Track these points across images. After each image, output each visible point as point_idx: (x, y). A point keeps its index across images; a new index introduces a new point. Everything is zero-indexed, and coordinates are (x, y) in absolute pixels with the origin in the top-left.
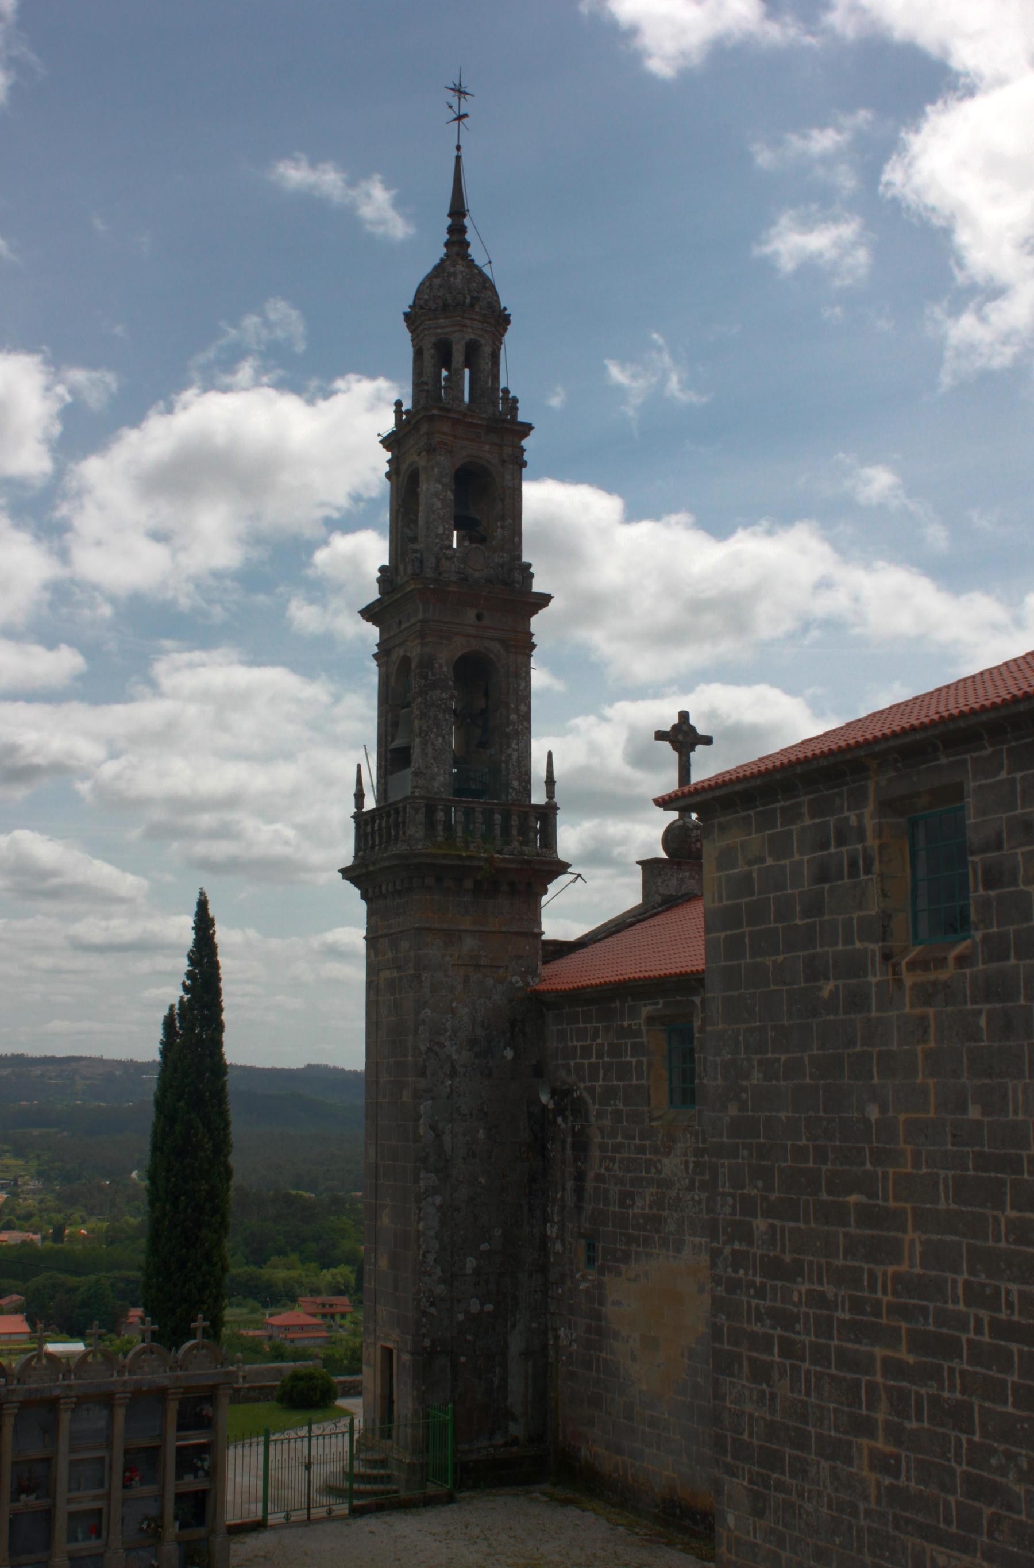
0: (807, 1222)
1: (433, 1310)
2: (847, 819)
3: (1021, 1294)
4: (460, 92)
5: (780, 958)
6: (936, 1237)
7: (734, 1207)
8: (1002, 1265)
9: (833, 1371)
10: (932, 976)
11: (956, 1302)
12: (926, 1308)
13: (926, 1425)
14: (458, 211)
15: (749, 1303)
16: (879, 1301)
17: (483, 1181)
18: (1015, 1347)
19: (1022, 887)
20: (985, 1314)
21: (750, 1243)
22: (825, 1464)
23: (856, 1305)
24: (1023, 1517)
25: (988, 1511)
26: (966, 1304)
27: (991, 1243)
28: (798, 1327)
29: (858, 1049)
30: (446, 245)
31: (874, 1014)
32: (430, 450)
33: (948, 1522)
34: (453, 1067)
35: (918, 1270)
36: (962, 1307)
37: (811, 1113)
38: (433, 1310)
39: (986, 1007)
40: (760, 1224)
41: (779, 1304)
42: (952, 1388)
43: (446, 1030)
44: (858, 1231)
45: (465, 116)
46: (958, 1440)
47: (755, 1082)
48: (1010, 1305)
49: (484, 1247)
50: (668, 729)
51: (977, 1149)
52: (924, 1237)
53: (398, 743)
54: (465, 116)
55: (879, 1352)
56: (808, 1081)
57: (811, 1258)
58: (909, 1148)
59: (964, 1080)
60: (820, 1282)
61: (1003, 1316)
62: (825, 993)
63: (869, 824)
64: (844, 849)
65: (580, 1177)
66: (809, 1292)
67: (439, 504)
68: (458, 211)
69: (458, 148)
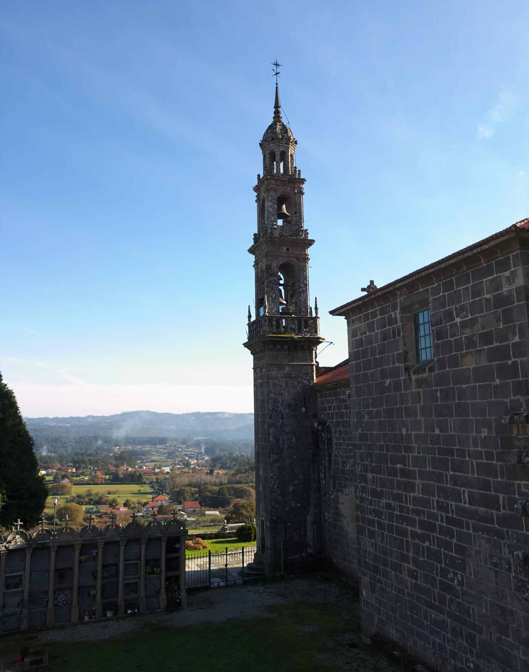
0: (384, 475)
1: (277, 506)
2: (391, 315)
3: (456, 506)
4: (277, 65)
5: (372, 371)
6: (426, 482)
7: (361, 469)
8: (449, 494)
9: (395, 536)
10: (421, 376)
11: (465, 503)
12: (424, 511)
13: (426, 559)
15: (367, 507)
16: (408, 507)
17: (295, 457)
19: (449, 339)
20: (443, 514)
21: (367, 483)
22: (393, 573)
23: (401, 509)
24: (460, 600)
25: (448, 597)
26: (438, 510)
27: (445, 485)
28: (383, 517)
29: (398, 406)
30: (274, 118)
31: (403, 392)
32: (268, 190)
33: (435, 600)
34: (282, 415)
35: (421, 495)
36: (436, 511)
37: (384, 432)
38: (277, 506)
39: (439, 388)
40: (370, 476)
41: (376, 508)
42: (434, 545)
43: (279, 401)
44: (401, 479)
45: (279, 73)
46: (437, 566)
47: (366, 420)
48: (452, 511)
49: (296, 482)
50: (366, 287)
51: (438, 446)
52: (422, 482)
53: (260, 297)
54: (279, 73)
55: (409, 528)
56: (383, 419)
57: (386, 490)
58: (416, 445)
59: (433, 418)
60: (390, 500)
61: (450, 515)
62: (387, 384)
63: (398, 317)
64: (391, 327)
65: (330, 455)
66: (386, 503)
67: (272, 210)
69: (277, 84)
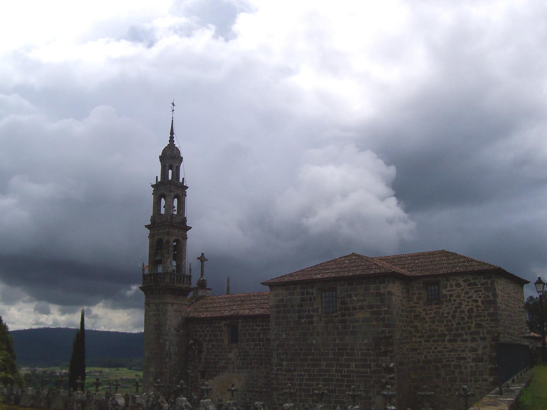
14: (172, 133)
18: (345, 378)
23: (309, 375)
40: (285, 363)
48: (345, 372)
68: (172, 133)
